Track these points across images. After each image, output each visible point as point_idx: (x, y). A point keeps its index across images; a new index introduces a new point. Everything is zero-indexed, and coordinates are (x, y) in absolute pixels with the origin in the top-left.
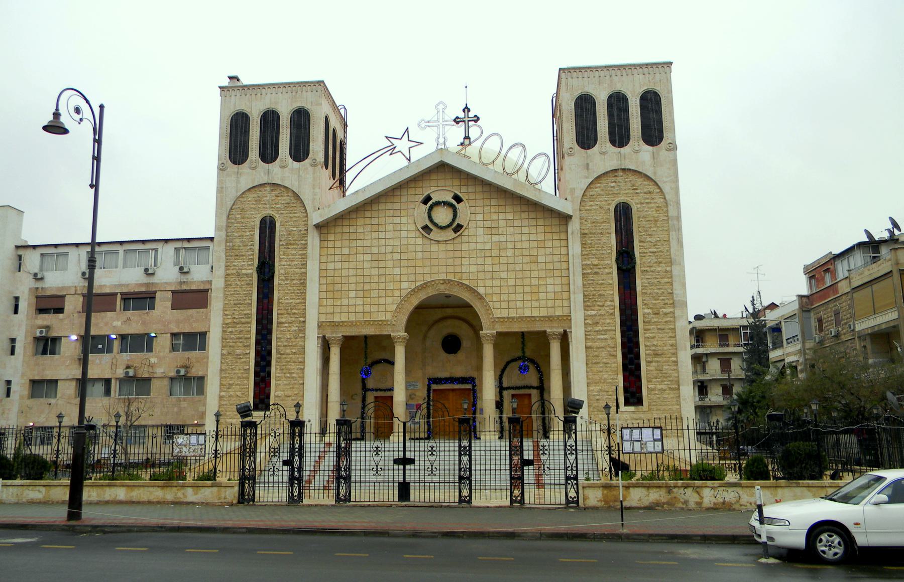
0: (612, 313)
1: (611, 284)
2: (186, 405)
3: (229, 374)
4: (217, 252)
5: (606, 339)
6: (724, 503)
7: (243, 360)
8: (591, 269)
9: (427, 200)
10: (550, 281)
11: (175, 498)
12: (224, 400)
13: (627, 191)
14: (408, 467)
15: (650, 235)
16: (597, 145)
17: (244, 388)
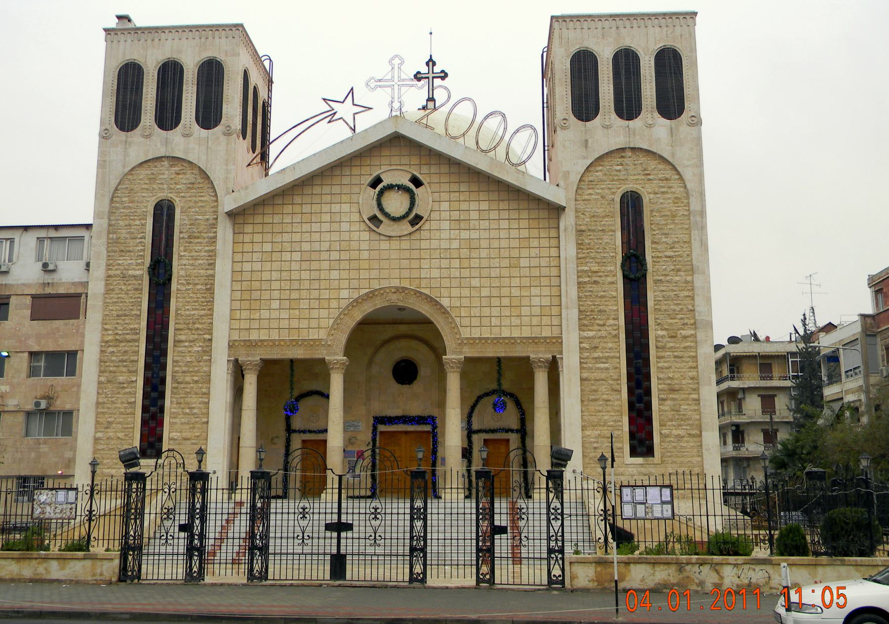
0: (616, 335)
1: (615, 297)
2: (46, 450)
5: (607, 369)
6: (749, 585)
7: (127, 390)
8: (589, 277)
11: (35, 574)
12: (101, 444)
13: (637, 177)
14: (343, 534)
15: (666, 234)
16: (598, 116)
17: (128, 428)
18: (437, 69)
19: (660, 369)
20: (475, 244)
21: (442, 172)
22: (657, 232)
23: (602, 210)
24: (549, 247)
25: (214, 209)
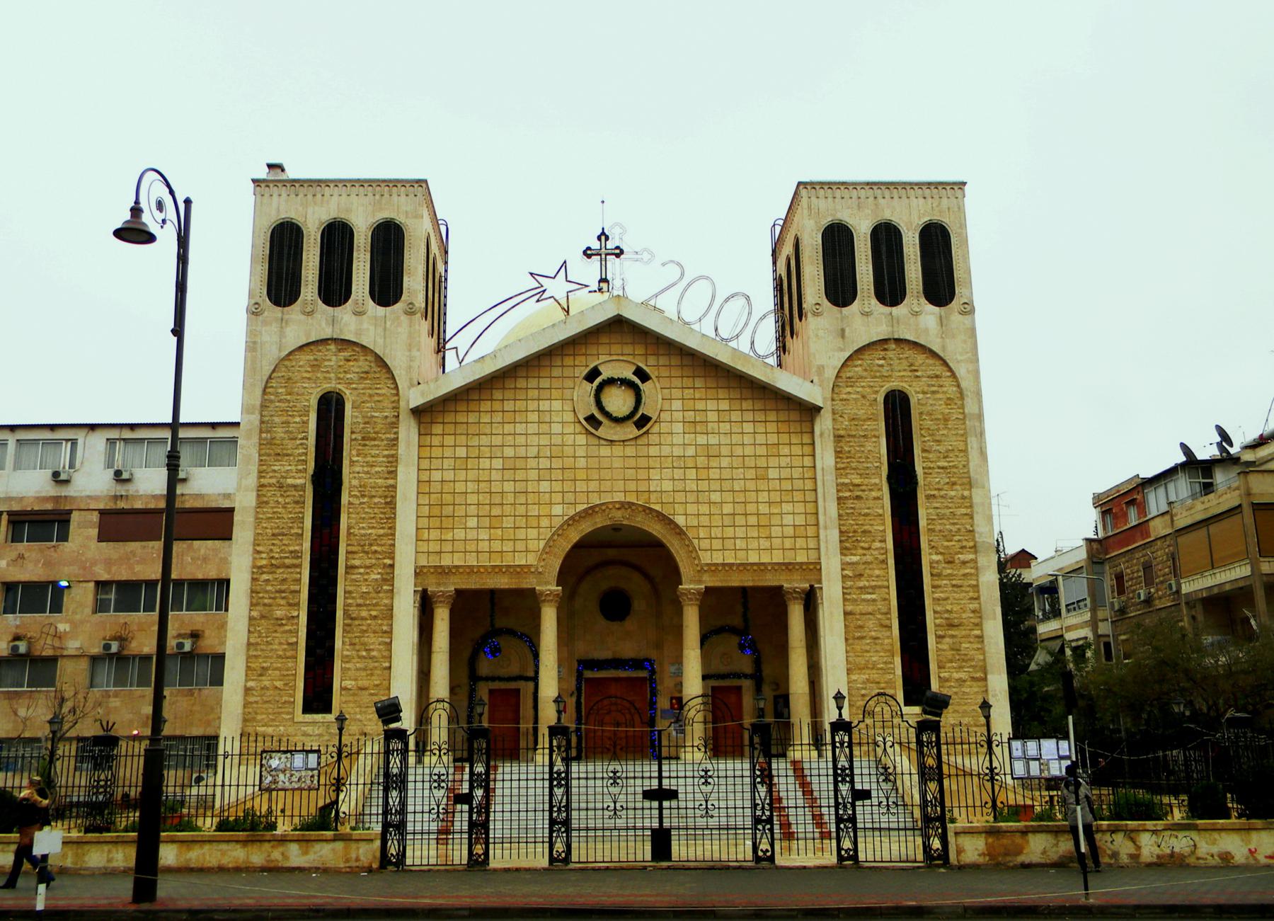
0: (883, 561)
1: (881, 515)
2: (118, 704)
3: (262, 650)
4: (248, 447)
5: (874, 600)
6: (1172, 855)
7: (287, 628)
8: (850, 491)
9: (592, 375)
10: (787, 507)
11: (268, 861)
12: (253, 695)
13: (902, 374)
14: (666, 804)
15: (938, 441)
16: (856, 301)
17: (287, 675)
18: (610, 245)
19: (936, 600)
20: (713, 452)
21: (672, 364)
22: (927, 438)
23: (864, 411)
24: (803, 456)
25: (394, 405)
